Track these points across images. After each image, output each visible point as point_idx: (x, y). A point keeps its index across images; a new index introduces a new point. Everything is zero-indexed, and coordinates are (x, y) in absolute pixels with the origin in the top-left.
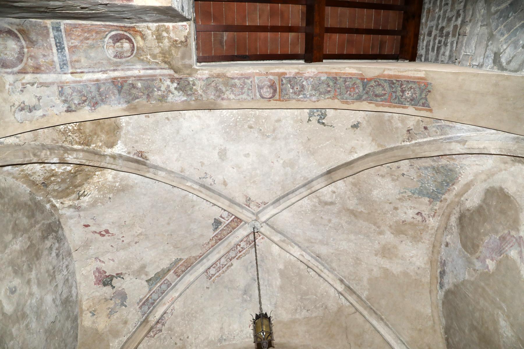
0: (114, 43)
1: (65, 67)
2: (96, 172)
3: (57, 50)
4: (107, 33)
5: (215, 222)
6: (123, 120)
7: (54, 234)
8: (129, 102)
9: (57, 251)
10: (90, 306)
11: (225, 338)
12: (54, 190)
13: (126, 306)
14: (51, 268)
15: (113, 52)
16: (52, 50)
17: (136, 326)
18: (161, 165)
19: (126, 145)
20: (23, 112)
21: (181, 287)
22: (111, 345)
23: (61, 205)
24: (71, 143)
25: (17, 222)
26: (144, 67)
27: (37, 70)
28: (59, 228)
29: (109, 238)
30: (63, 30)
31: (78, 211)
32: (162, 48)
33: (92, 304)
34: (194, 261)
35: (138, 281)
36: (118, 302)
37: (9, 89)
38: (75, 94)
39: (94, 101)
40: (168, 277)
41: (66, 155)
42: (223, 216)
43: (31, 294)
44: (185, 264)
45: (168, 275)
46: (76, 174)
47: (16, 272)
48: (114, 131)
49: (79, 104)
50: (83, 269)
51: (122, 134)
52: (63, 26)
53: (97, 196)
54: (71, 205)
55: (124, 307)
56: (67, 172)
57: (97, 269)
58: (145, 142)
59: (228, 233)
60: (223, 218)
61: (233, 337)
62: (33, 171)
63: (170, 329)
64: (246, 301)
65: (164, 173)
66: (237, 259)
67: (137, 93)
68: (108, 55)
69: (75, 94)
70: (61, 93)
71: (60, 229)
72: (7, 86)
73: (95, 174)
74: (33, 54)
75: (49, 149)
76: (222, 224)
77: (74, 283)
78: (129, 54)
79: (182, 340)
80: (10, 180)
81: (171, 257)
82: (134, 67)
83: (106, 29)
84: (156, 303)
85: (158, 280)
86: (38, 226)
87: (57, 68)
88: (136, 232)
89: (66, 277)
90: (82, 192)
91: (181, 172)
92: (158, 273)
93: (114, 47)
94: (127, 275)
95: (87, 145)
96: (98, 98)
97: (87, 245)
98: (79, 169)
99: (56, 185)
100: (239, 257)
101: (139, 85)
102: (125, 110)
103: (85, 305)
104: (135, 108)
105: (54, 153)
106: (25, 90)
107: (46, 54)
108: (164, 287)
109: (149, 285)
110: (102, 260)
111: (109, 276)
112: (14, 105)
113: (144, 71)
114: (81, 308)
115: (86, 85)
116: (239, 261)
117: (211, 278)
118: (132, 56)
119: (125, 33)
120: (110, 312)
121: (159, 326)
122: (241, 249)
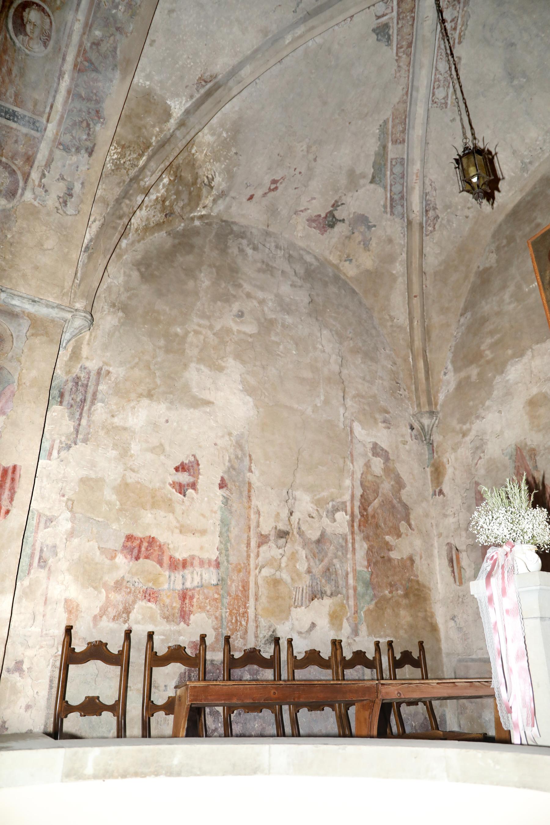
0: (26, 34)
1: (37, 125)
2: (190, 152)
3: (14, 121)
4: (8, 36)
5: (377, 34)
6: (141, 81)
7: (230, 237)
8: (116, 66)
9: (251, 246)
10: (340, 256)
11: (528, 161)
12: (182, 208)
13: (375, 226)
14: (259, 265)
15: (38, 43)
16: (12, 128)
17: (404, 235)
18: (235, 61)
19: (178, 95)
20: (69, 204)
21: (416, 154)
22: (394, 272)
23: (206, 209)
24: (134, 166)
25: (184, 267)
26: (75, 8)
27: (30, 160)
28: (230, 226)
29: (284, 185)
31: (227, 196)
33: (338, 253)
34: (404, 105)
35: (361, 191)
36: (363, 228)
37: (39, 203)
38: (74, 132)
39: (93, 113)
40: (391, 155)
41: (142, 183)
42: (379, 14)
43: (262, 302)
44: (397, 121)
45: (389, 153)
46: (179, 175)
47: (227, 301)
48: (150, 101)
49: (88, 134)
50: (295, 233)
51: (159, 92)
53: (223, 166)
54: (214, 200)
55: (373, 228)
56: (169, 184)
57: (308, 220)
58: (189, 66)
59: (413, 25)
60: (383, 15)
61: (540, 151)
62: (144, 219)
63: (447, 207)
64: (522, 87)
65: (248, 66)
66: (460, 42)
67: (109, 45)
69: (74, 132)
70: (67, 149)
71: (232, 226)
72: (36, 203)
73: (193, 155)
74: (10, 154)
75: (124, 198)
76: (391, 25)
77: (301, 252)
79: (472, 207)
80: (140, 247)
81: (371, 132)
82: (69, 24)
84: (405, 194)
85: (383, 169)
86: (207, 250)
87: (35, 135)
88: (302, 151)
89: (287, 255)
90: (206, 181)
91: (266, 35)
92: (375, 163)
93: (31, 38)
94: (343, 198)
95: (148, 148)
96: (92, 105)
97: (273, 211)
98: (175, 170)
99: (177, 203)
100: (460, 36)
101: (98, 33)
102: (123, 79)
103: (333, 259)
104: (128, 62)
105: (132, 195)
106: (47, 187)
107: (15, 139)
108: (397, 170)
109: (379, 184)
110: (302, 208)
111: (326, 215)
112: (58, 209)
113: (79, 13)
114: (333, 265)
115: (69, 111)
116: (464, 44)
117: (446, 104)
118: (52, 18)
120: (364, 244)
121: (431, 214)
122: (453, 24)
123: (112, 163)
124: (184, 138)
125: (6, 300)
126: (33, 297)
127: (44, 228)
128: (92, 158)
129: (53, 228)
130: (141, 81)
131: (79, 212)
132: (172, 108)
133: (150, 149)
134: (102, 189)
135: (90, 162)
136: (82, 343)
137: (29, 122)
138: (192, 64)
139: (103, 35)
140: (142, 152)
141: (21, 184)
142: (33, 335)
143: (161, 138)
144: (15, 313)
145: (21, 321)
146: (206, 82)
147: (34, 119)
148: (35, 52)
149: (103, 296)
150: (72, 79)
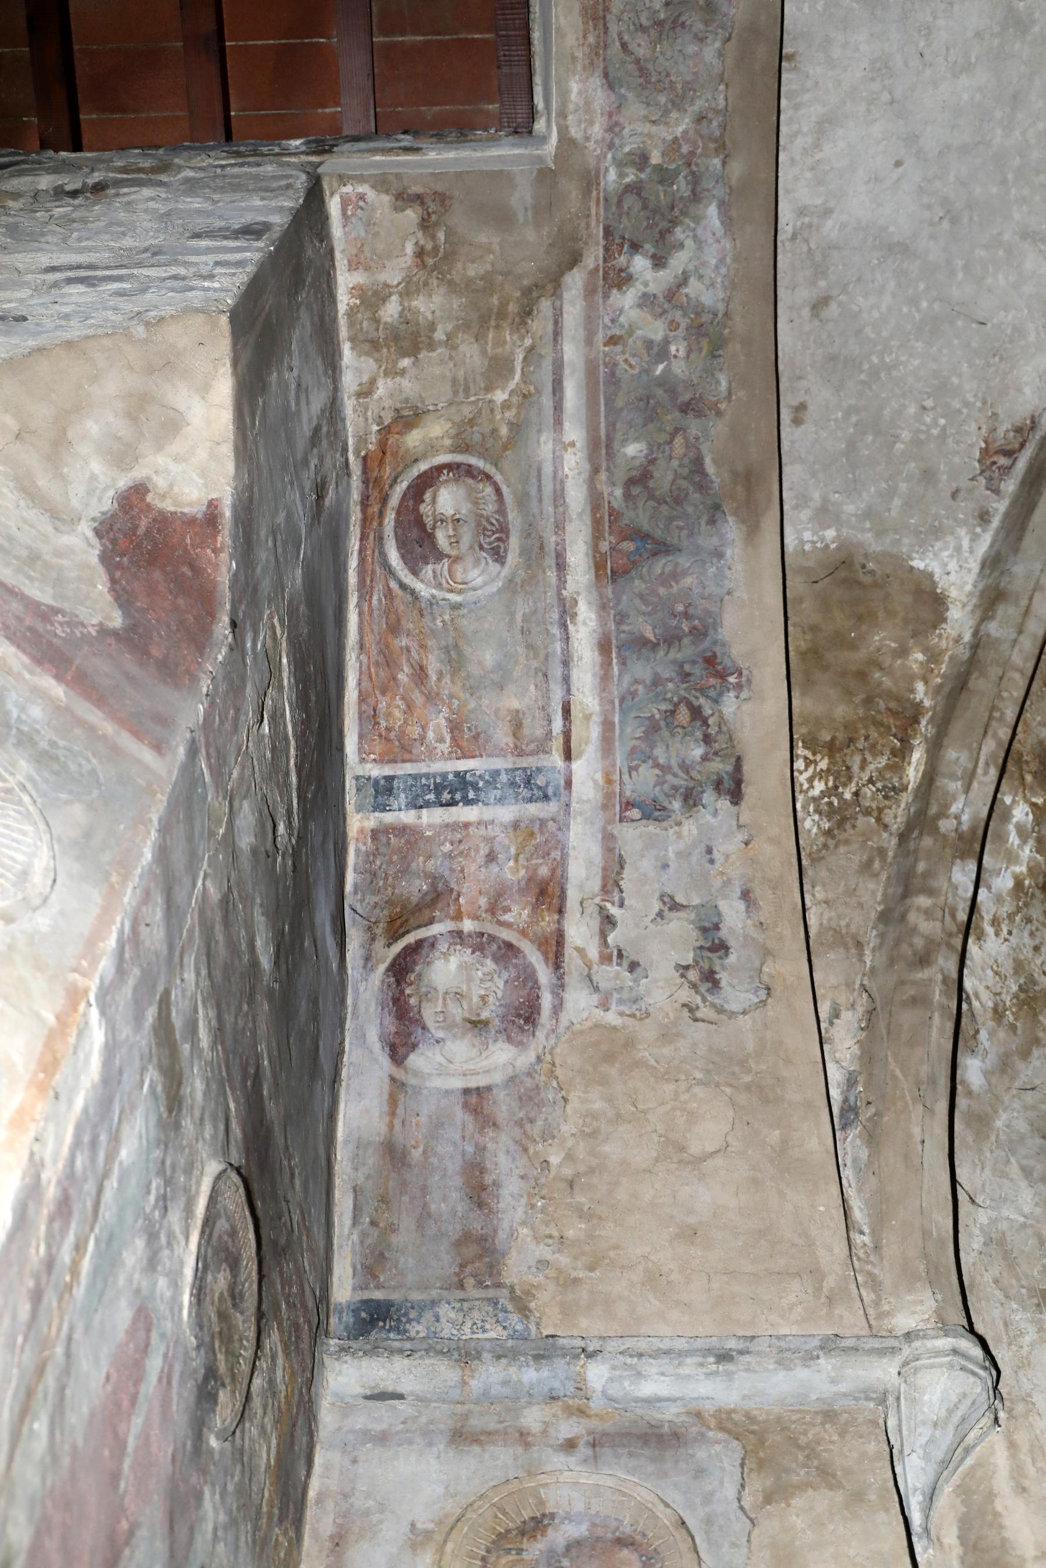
0: (440, 556)
1: (540, 781)
3: (468, 802)
4: (393, 585)
6: (807, 535)
8: (717, 507)
15: (477, 562)
16: (467, 825)
19: (937, 532)
20: (723, 977)
24: (891, 793)
30: (388, 770)
32: (457, 328)
37: (621, 1014)
39: (698, 670)
41: (946, 825)
48: (859, 584)
49: (707, 739)
52: (369, 766)
58: (935, 432)
62: (1007, 968)
67: (675, 463)
68: (494, 588)
69: (659, 753)
72: (611, 1018)
74: (483, 901)
75: (905, 895)
78: (489, 490)
82: (548, 469)
83: (379, 587)
87: (542, 815)
93: (457, 559)
96: (687, 651)
101: (633, 449)
102: (752, 531)
105: (927, 874)
107: (484, 851)
113: (567, 425)
115: (622, 700)
118: (498, 478)
119: (394, 501)
123: (818, 811)
124: (1020, 632)
125: (614, 1391)
126: (714, 1342)
127: (670, 1087)
128: (743, 804)
129: (699, 1075)
130: (807, 535)
131: (768, 989)
132: (936, 578)
133: (924, 723)
134: (818, 903)
135: (744, 818)
136: (991, 1496)
137: (513, 784)
138: (942, 421)
139: (650, 446)
140: (901, 740)
141: (544, 975)
142: (768, 1499)
143: (943, 676)
144: (666, 1429)
145: (701, 1454)
146: (1009, 453)
147: (524, 769)
148: (475, 589)
149: (988, 1277)
150: (603, 607)
